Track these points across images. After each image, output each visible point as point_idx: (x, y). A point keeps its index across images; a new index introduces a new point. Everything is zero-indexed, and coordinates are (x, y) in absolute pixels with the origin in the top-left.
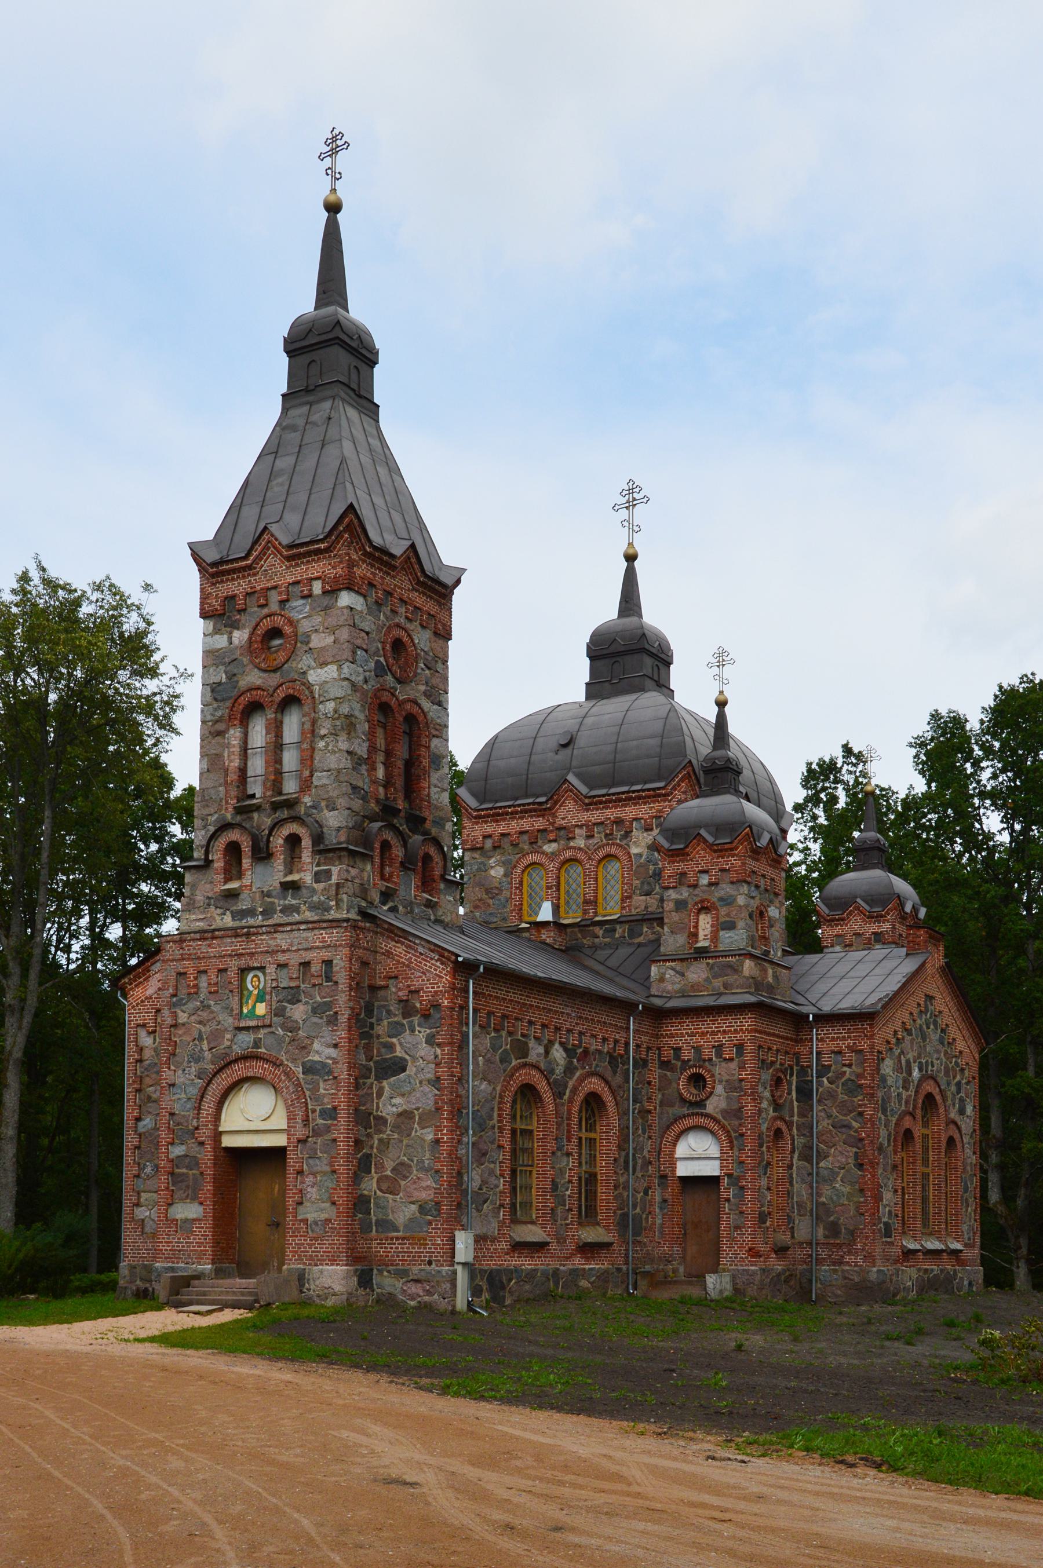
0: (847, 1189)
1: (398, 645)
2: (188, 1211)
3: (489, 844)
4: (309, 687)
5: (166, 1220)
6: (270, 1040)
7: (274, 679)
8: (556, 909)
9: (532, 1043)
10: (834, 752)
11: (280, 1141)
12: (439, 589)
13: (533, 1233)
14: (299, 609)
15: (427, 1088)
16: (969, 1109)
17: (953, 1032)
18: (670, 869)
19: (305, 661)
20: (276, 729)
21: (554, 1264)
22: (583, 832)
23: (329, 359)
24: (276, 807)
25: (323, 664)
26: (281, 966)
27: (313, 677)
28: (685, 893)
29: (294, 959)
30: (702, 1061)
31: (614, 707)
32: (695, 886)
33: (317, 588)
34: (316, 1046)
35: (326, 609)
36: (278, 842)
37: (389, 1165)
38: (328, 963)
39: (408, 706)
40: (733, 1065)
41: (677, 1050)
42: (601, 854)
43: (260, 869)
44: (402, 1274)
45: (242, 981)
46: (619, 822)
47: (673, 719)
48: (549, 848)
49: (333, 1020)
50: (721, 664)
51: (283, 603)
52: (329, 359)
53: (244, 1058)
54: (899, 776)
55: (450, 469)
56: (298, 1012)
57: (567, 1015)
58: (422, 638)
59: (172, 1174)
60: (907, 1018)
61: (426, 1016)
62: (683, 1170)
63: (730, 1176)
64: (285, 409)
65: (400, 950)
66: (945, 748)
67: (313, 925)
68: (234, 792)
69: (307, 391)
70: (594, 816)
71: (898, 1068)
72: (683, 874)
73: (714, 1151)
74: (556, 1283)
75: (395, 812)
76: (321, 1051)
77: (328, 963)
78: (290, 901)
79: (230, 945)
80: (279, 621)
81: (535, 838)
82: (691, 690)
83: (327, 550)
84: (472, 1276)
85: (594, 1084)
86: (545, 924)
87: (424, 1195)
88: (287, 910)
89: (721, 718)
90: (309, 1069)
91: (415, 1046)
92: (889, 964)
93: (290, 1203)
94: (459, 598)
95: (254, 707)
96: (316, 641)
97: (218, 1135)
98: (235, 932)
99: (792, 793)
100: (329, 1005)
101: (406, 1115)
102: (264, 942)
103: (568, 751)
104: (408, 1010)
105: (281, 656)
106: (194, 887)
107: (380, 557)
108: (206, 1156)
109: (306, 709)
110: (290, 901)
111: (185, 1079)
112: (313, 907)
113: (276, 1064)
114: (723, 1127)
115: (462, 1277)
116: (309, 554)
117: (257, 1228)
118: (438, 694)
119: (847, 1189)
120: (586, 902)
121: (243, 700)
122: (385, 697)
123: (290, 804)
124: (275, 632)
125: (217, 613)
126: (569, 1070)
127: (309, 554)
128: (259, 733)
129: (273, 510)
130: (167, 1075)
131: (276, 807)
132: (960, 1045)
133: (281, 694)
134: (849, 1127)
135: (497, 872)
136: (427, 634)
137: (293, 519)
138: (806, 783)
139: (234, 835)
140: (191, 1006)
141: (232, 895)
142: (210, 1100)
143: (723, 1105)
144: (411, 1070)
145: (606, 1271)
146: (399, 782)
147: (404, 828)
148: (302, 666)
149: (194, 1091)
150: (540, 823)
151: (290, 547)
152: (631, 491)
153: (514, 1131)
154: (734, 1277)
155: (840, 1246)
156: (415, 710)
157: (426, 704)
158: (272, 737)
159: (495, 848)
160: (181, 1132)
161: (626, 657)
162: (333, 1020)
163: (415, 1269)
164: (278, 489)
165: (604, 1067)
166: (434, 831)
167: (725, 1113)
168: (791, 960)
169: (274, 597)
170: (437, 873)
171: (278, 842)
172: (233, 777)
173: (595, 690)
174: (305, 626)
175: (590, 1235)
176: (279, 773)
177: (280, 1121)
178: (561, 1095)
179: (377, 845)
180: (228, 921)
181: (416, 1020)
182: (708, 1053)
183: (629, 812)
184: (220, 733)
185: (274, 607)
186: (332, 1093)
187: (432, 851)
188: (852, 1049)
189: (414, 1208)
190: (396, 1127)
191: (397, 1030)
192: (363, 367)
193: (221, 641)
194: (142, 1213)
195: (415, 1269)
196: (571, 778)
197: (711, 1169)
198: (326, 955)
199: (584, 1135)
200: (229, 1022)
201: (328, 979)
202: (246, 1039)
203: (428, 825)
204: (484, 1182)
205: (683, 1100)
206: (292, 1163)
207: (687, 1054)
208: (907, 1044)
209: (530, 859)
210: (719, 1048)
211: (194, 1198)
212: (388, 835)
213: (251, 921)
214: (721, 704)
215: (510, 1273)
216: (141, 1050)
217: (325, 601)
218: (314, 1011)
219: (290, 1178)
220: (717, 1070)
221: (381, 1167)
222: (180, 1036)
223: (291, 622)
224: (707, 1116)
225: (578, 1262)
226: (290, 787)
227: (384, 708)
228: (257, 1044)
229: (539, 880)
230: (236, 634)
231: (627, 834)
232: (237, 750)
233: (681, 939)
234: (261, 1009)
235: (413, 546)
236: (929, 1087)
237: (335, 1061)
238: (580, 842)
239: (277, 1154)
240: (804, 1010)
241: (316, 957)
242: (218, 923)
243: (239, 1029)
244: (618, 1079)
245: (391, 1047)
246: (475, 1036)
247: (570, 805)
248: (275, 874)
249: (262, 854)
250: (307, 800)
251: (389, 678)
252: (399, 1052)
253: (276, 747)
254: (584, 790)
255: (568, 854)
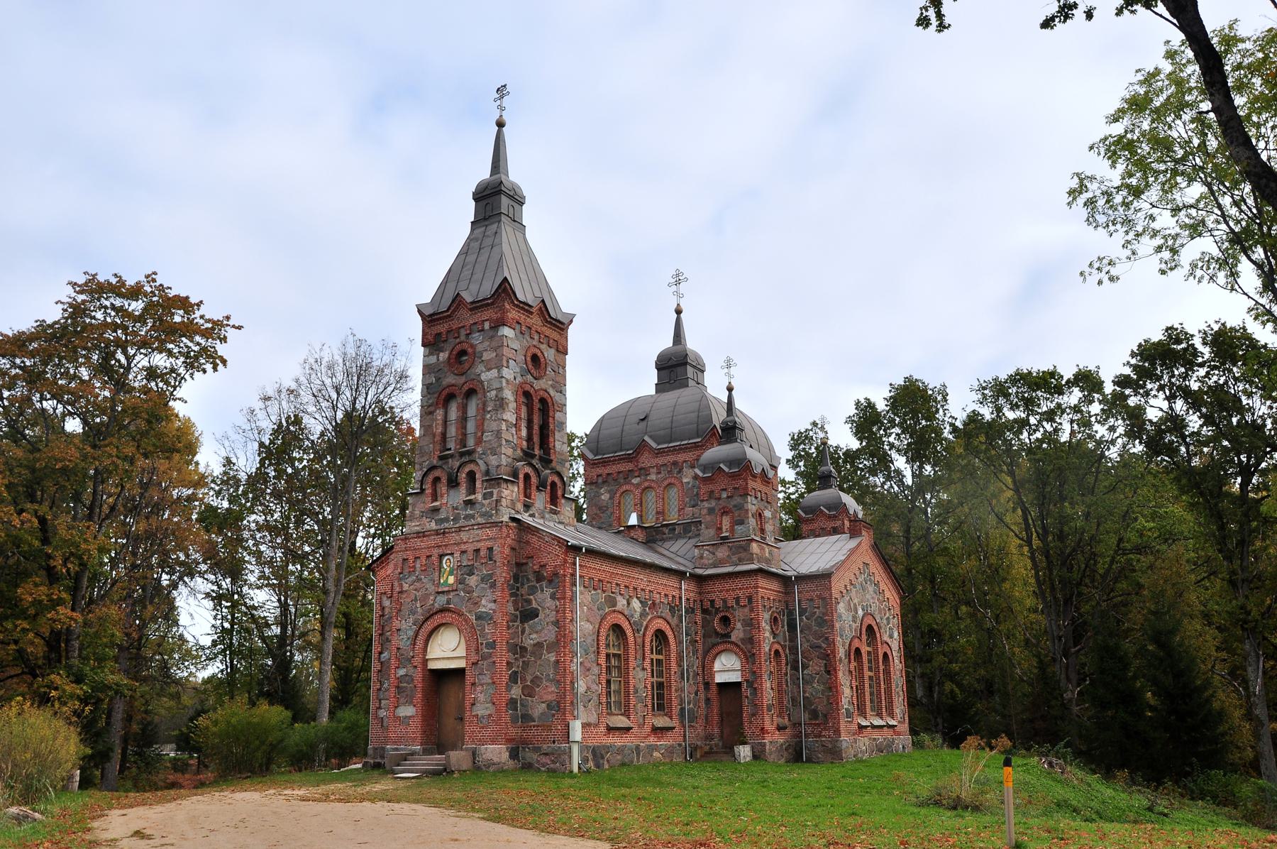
0: (821, 688)
1: (535, 359)
2: (407, 711)
3: (600, 480)
4: (482, 382)
5: (402, 716)
6: (456, 600)
7: (463, 379)
8: (640, 517)
9: (619, 598)
10: (804, 425)
11: (461, 664)
12: (560, 326)
13: (621, 721)
14: (477, 338)
15: (551, 627)
16: (896, 634)
17: (883, 586)
18: (704, 489)
19: (480, 368)
20: (464, 409)
21: (636, 742)
22: (654, 470)
23: (495, 201)
24: (462, 454)
25: (489, 370)
26: (463, 552)
27: (483, 377)
28: (713, 503)
29: (470, 548)
30: (727, 608)
31: (671, 397)
32: (719, 499)
33: (487, 326)
34: (483, 602)
35: (492, 337)
36: (463, 476)
37: (529, 678)
38: (490, 549)
39: (541, 393)
40: (746, 610)
41: (712, 602)
42: (666, 483)
43: (452, 492)
44: (537, 750)
45: (441, 562)
46: (675, 463)
47: (704, 401)
48: (635, 481)
49: (493, 586)
50: (729, 366)
51: (468, 335)
52: (495, 201)
53: (442, 611)
54: (844, 438)
55: (559, 254)
56: (473, 581)
57: (642, 579)
58: (550, 354)
59: (398, 687)
60: (852, 577)
61: (550, 581)
62: (719, 679)
63: (747, 681)
64: (472, 230)
65: (535, 539)
66: (866, 421)
67: (481, 526)
68: (438, 447)
69: (485, 219)
70: (660, 461)
71: (849, 609)
72: (712, 492)
73: (738, 665)
74: (638, 755)
75: (533, 456)
76: (486, 606)
77: (490, 549)
78: (470, 512)
79: (433, 541)
80: (465, 346)
81: (628, 475)
82: (714, 384)
83: (492, 304)
84: (581, 751)
85: (660, 624)
86: (634, 526)
87: (550, 697)
88: (467, 517)
89: (730, 398)
90: (479, 617)
91: (544, 600)
92: (839, 545)
93: (467, 703)
94: (572, 331)
95: (451, 397)
96: (486, 356)
97: (425, 661)
98: (437, 533)
99: (783, 452)
100: (491, 576)
101: (539, 645)
102: (454, 538)
103: (644, 423)
104: (539, 578)
105: (466, 366)
106: (414, 505)
107: (525, 307)
108: (418, 675)
109: (480, 396)
110: (470, 512)
111: (406, 625)
112: (482, 515)
113: (460, 614)
114: (741, 650)
115: (575, 750)
116: (482, 306)
117: (449, 722)
118: (560, 386)
119: (821, 688)
120: (658, 513)
121: (445, 393)
122: (528, 388)
123: (470, 453)
124: (463, 353)
125: (431, 343)
126: (643, 615)
127: (482, 306)
128: (454, 413)
129: (463, 285)
130: (396, 623)
131: (462, 454)
132: (888, 594)
133: (466, 388)
134: (820, 647)
135: (605, 497)
136: (552, 351)
137: (474, 287)
138: (793, 448)
139: (437, 473)
140: (410, 579)
141: (436, 510)
142: (421, 638)
143: (741, 635)
144: (541, 616)
145: (672, 746)
146: (536, 439)
147: (538, 466)
148: (478, 371)
149: (411, 633)
150: (630, 466)
151: (472, 303)
152: (677, 275)
153: (608, 656)
154: (753, 748)
155: (818, 725)
156: (546, 395)
157: (552, 393)
158: (460, 413)
159: (604, 482)
160: (403, 660)
161: (676, 367)
162: (493, 586)
163: (545, 746)
164: (467, 273)
165: (666, 612)
166: (559, 468)
167: (742, 640)
168: (780, 545)
169: (463, 332)
170: (560, 493)
171: (463, 476)
172: (438, 438)
173: (660, 387)
174: (480, 348)
175: (661, 721)
176: (465, 435)
177: (462, 652)
178: (638, 631)
179: (521, 476)
180: (433, 525)
181: (544, 583)
182: (731, 603)
183: (680, 458)
184: (431, 413)
185: (463, 338)
186: (495, 632)
187: (556, 479)
188: (820, 597)
189: (544, 705)
190: (533, 653)
191: (533, 590)
192: (516, 206)
193: (433, 359)
194: (382, 713)
195: (545, 746)
196: (646, 438)
197: (735, 677)
198: (489, 544)
199: (655, 657)
200: (432, 588)
201: (491, 559)
202: (442, 600)
203: (553, 464)
204: (588, 688)
205: (717, 633)
206: (469, 678)
207: (719, 604)
208: (853, 594)
209: (624, 488)
210: (737, 599)
211: (411, 703)
212: (528, 470)
213: (446, 525)
214: (730, 389)
215: (608, 748)
216: (383, 609)
217: (491, 333)
218: (482, 580)
219: (468, 688)
220: (737, 613)
221: (524, 679)
222: (405, 599)
223: (472, 346)
224: (733, 643)
225: (652, 740)
226: (471, 443)
227: (527, 394)
228: (448, 602)
229: (630, 500)
230: (441, 355)
231: (680, 471)
232: (440, 422)
233: (712, 532)
234: (451, 580)
235: (543, 301)
236: (869, 621)
237: (495, 611)
238: (653, 477)
239: (460, 672)
240: (789, 574)
241: (483, 546)
242: (428, 527)
243: (438, 593)
244: (674, 621)
245: (529, 602)
246: (581, 593)
247: (646, 454)
248: (461, 495)
249: (453, 483)
250: (479, 450)
251: (529, 377)
252: (534, 605)
253: (463, 419)
254: (654, 445)
255: (646, 484)
